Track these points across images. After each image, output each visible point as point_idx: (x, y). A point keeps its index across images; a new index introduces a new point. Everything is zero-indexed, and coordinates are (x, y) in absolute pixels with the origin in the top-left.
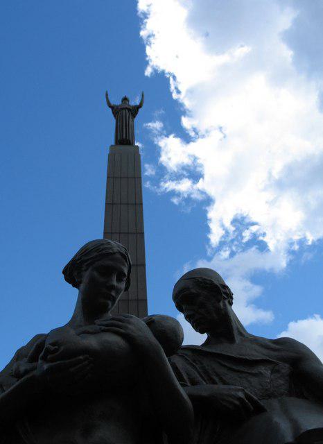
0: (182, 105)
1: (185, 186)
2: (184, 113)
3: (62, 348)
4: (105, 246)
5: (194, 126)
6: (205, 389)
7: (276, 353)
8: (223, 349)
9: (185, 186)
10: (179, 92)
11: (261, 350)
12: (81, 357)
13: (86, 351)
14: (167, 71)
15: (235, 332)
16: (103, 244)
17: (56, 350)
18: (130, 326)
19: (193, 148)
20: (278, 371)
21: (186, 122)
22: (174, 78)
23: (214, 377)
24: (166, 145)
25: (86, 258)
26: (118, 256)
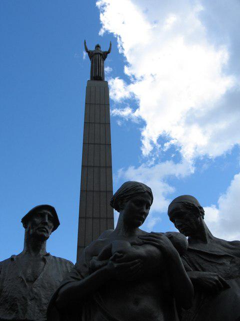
0: (125, 58)
1: (127, 112)
2: (127, 64)
3: (125, 256)
4: (139, 188)
5: (133, 74)
6: (196, 274)
7: (232, 251)
8: (199, 247)
9: (127, 112)
10: (123, 49)
11: (221, 247)
12: (136, 261)
13: (139, 257)
14: (115, 34)
15: (207, 237)
16: (137, 186)
17: (122, 256)
18: (161, 241)
19: (132, 88)
20: (234, 262)
21: (127, 71)
22: (120, 37)
23: (197, 266)
24: (113, 83)
25: (127, 195)
26: (147, 194)
